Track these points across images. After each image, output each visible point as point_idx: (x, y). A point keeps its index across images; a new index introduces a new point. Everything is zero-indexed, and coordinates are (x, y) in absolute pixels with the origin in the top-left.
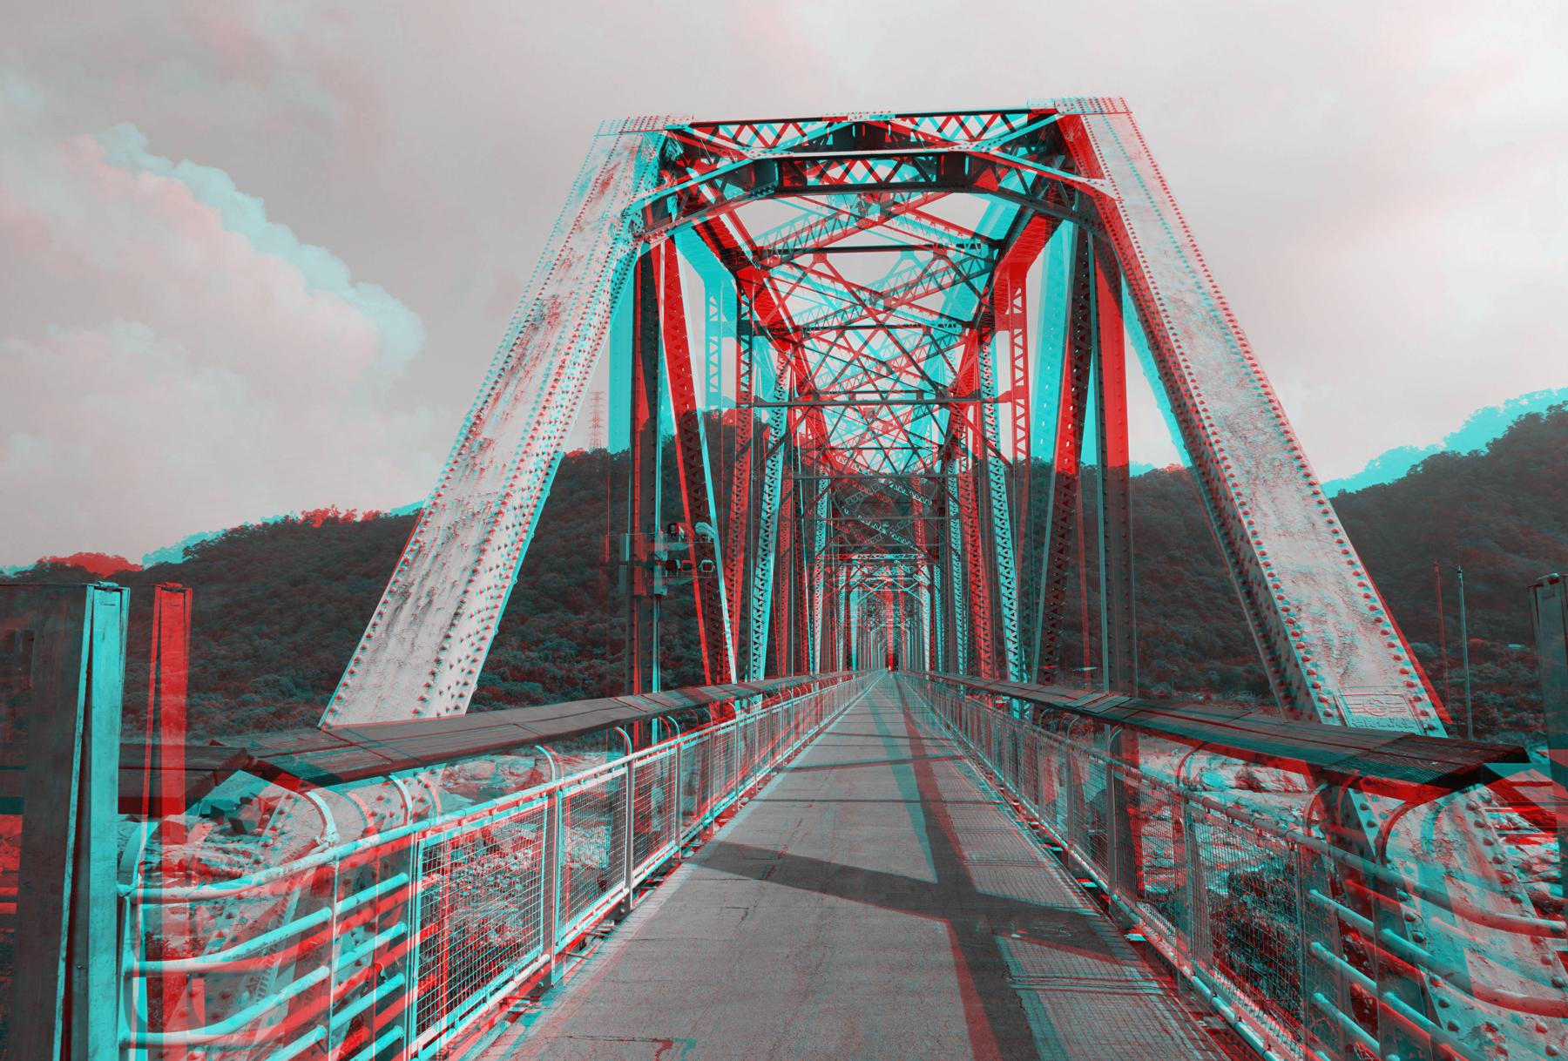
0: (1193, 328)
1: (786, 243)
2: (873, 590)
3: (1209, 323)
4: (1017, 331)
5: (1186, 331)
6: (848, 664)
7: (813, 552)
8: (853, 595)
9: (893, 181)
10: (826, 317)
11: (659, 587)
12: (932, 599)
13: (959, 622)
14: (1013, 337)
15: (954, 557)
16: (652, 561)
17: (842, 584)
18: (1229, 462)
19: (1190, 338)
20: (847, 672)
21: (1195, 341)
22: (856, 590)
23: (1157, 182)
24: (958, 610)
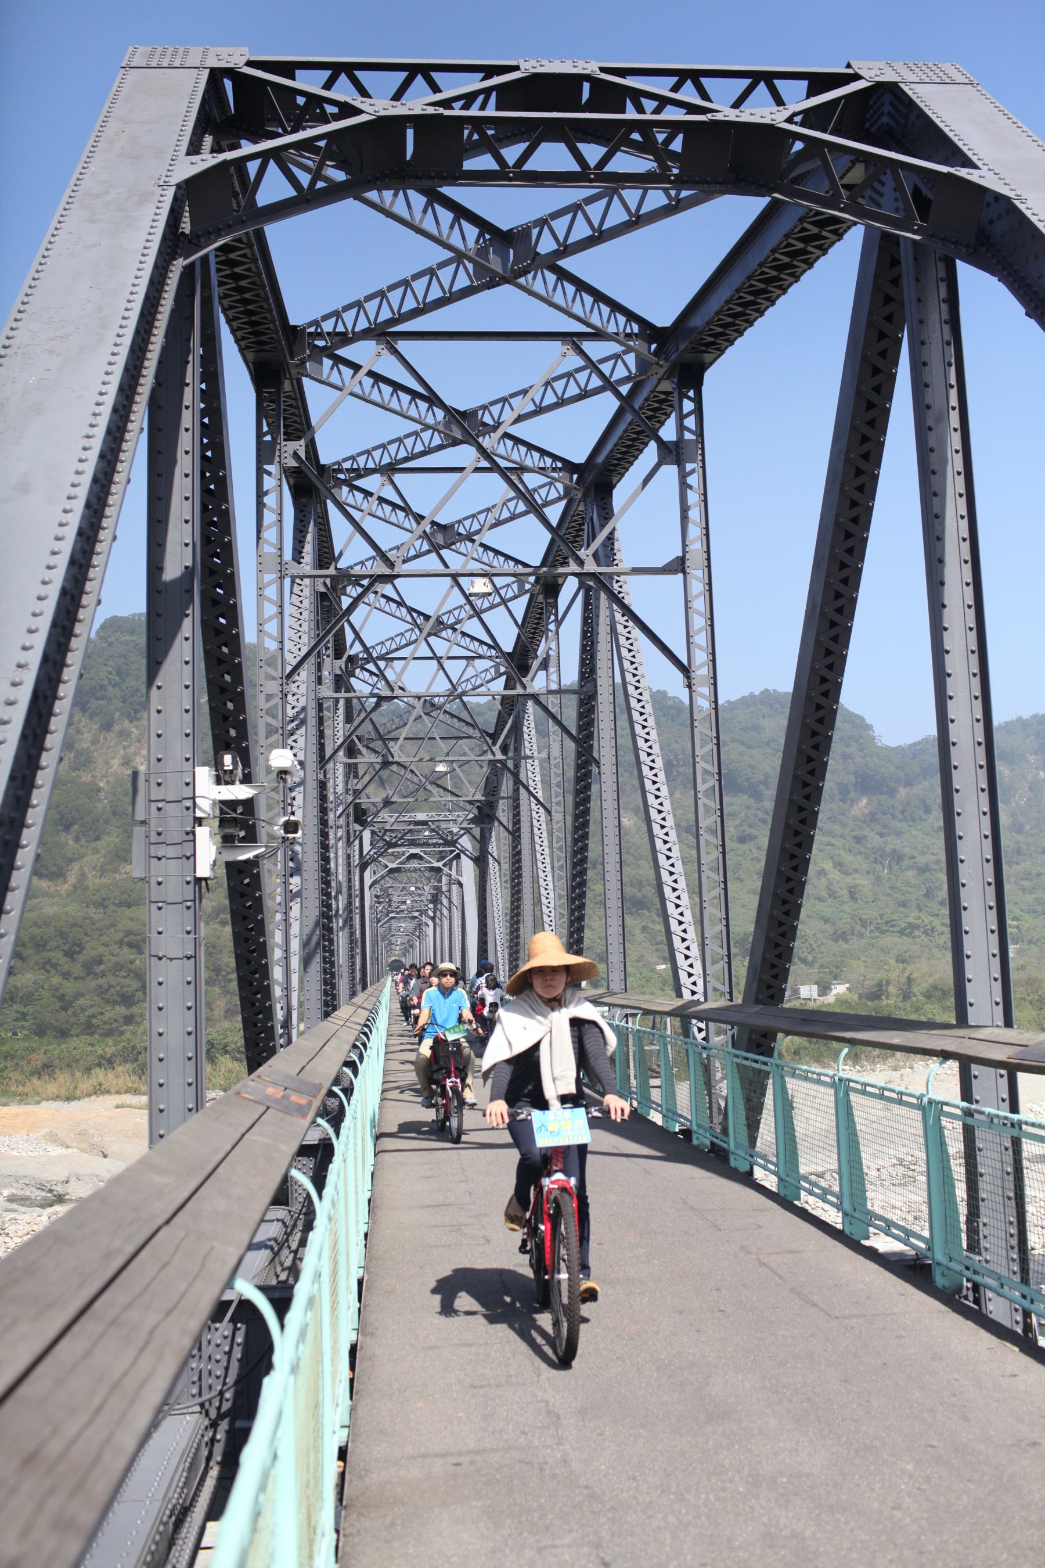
8: (367, 874)
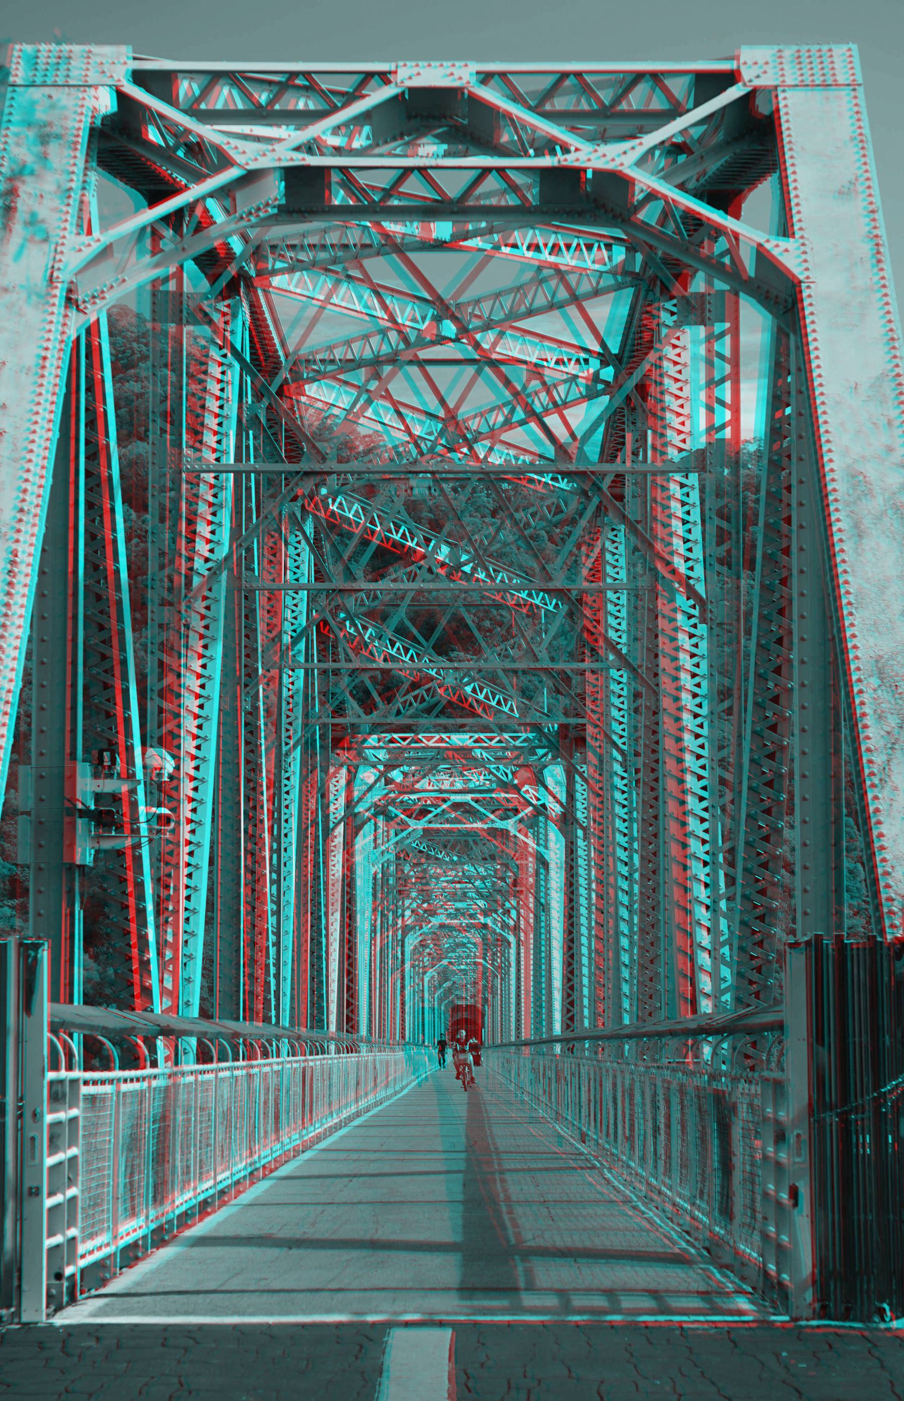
0: (867, 522)
1: (332, 352)
2: (417, 826)
3: (890, 512)
4: (719, 327)
5: (857, 525)
6: (349, 1021)
7: (304, 753)
8: (363, 841)
9: (564, 800)
10: (348, 343)
11: (85, 855)
12: (571, 850)
13: (702, 914)
14: (711, 339)
15: (682, 601)
16: (72, 811)
17: (337, 808)
18: (866, 697)
19: (860, 536)
20: (185, 1177)
21: (864, 541)
22: (368, 828)
23: (385, 1233)
24: (698, 870)
